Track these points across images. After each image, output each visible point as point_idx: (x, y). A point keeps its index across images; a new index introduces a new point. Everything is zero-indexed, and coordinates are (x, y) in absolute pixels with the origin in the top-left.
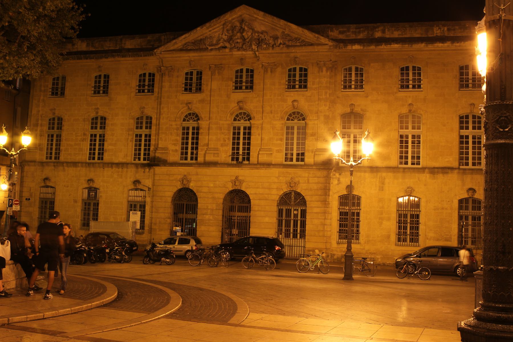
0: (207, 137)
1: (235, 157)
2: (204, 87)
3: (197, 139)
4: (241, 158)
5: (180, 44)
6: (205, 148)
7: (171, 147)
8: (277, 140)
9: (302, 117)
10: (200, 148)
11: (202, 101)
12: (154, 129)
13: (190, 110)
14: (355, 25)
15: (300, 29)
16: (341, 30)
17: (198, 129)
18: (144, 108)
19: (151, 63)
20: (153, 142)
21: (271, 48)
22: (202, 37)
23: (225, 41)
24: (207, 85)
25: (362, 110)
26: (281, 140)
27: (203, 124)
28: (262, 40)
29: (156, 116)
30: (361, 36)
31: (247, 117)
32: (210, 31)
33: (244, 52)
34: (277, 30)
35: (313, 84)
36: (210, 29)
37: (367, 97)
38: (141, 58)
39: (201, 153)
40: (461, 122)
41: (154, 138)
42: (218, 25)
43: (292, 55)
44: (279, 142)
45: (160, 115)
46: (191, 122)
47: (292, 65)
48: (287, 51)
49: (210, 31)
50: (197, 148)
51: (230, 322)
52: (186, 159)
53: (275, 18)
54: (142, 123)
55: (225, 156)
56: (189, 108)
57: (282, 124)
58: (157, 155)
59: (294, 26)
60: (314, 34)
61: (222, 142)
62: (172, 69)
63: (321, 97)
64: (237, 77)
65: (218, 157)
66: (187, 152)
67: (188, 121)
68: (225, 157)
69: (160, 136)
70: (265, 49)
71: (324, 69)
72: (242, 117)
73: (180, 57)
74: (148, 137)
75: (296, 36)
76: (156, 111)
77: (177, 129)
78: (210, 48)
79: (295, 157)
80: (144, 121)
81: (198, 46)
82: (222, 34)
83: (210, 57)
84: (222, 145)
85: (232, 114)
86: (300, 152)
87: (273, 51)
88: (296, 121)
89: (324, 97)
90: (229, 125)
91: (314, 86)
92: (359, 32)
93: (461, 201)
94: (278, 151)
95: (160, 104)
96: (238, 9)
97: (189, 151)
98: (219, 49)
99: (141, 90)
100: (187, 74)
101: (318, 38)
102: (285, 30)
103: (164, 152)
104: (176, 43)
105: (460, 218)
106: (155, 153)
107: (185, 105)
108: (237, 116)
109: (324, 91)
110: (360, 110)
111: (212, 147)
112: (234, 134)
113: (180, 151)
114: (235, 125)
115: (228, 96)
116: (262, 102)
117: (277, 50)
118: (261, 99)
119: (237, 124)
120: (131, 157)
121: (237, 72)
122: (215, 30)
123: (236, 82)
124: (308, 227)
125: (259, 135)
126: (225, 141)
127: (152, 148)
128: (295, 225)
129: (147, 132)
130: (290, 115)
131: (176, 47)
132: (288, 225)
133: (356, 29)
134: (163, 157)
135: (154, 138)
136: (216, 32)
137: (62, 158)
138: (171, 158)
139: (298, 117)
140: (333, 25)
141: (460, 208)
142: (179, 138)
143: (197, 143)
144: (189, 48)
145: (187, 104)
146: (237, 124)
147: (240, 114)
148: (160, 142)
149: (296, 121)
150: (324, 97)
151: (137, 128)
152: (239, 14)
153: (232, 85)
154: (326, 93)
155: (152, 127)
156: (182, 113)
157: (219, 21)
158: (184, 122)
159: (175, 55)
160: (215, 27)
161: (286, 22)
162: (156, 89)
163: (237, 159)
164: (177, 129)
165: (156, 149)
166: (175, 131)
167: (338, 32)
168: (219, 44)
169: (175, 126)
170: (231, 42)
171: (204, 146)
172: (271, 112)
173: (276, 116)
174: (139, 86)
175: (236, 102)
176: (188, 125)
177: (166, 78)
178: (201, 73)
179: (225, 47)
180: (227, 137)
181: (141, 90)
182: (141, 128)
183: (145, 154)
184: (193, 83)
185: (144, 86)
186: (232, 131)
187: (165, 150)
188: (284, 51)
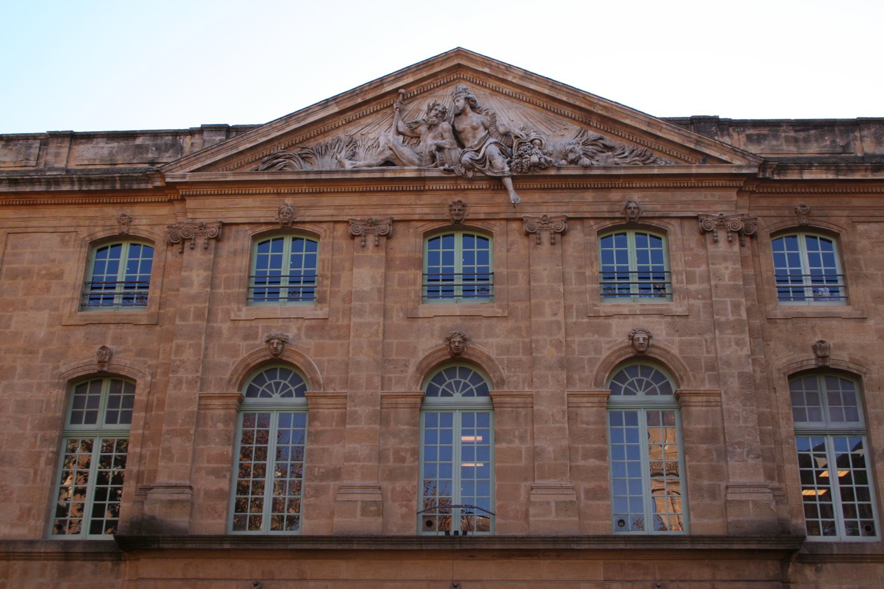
8: (585, 457)
24: (335, 280)
35: (690, 279)
44: (593, 462)
63: (723, 319)
66: (797, 256)
68: (403, 517)
71: (722, 235)
89: (731, 317)
91: (693, 287)
120: (47, 521)
125: (522, 438)
126: (403, 460)
139: (648, 384)
165: (144, 491)
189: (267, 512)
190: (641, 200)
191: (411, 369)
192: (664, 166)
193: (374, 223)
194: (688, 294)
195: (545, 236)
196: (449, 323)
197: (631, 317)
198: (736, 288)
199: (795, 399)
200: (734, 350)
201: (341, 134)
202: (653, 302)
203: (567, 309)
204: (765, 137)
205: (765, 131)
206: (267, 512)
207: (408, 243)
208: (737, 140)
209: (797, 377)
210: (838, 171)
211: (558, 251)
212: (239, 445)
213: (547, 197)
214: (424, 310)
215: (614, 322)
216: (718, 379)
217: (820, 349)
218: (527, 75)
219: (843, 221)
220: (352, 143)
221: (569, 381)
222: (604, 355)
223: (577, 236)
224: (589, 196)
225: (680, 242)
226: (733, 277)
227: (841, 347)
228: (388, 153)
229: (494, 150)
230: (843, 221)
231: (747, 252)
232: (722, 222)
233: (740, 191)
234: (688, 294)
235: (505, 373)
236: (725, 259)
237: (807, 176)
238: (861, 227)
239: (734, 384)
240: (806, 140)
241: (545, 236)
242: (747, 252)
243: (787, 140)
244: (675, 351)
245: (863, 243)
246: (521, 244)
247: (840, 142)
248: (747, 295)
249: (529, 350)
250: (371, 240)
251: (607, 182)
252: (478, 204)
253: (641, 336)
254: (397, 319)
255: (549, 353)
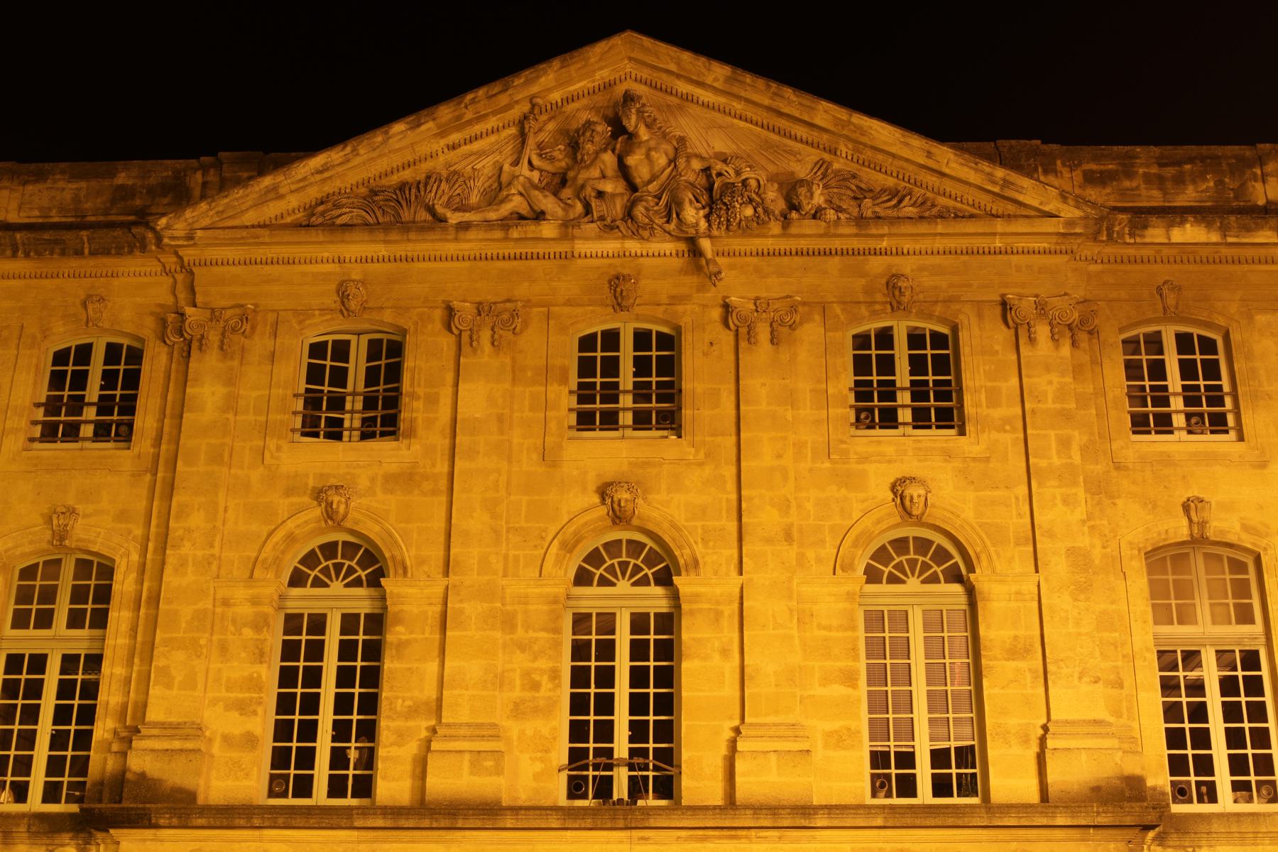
0: (433, 667)
1: (587, 777)
2: (412, 410)
3: (372, 677)
4: (621, 777)
5: (293, 201)
6: (422, 725)
7: (221, 722)
8: (826, 681)
9: (952, 563)
10: (387, 725)
11: (406, 479)
12: (124, 627)
13: (339, 526)
14: (1155, 150)
15: (917, 142)
16: (1093, 166)
17: (376, 622)
18: (72, 511)
19: (127, 294)
20: (109, 697)
21: (775, 228)
22: (407, 175)
23: (536, 187)
24: (432, 400)
25: (1245, 528)
26: (849, 679)
27: (411, 597)
28: (728, 187)
29: (135, 557)
30: (1189, 196)
31: (649, 562)
32: (454, 147)
33: (633, 246)
34: (791, 152)
36: (455, 137)
37: (1263, 465)
38: (74, 264)
39: (394, 751)
41: (120, 671)
42: (492, 122)
43: (877, 265)
44: (838, 690)
45: (162, 549)
46: (337, 587)
47: (874, 314)
48: (856, 244)
49: (454, 147)
50: (368, 731)
52: (304, 787)
53: (788, 92)
54: (49, 595)
55: (538, 767)
56: (330, 514)
57: (850, 596)
58: (137, 763)
59: (883, 133)
60: (985, 166)
61: (517, 693)
62: (244, 318)
63: (1043, 463)
64: (586, 367)
65: (498, 771)
67: (318, 583)
68: (536, 776)
69: (158, 662)
70: (745, 229)
72: (624, 565)
73: (290, 262)
74: (82, 676)
75: (890, 182)
76: (138, 531)
77: (259, 624)
78: (454, 218)
79: (924, 772)
80: (66, 582)
81: (397, 208)
82: (516, 163)
83: (445, 266)
84: (518, 711)
85: (568, 547)
86: (953, 744)
87: (783, 244)
88: (913, 584)
90: (555, 601)
91: (997, 413)
92: (1180, 181)
94: (839, 740)
95: (170, 488)
96: (600, 47)
97: (324, 745)
98: (505, 224)
99: (57, 425)
100: (317, 350)
101: (1006, 183)
102: (833, 152)
103: (177, 744)
104: (274, 193)
106: (124, 754)
107: (306, 499)
108: (594, 558)
109: (1052, 433)
110: (1237, 527)
111: (464, 719)
112: (580, 650)
113: (267, 745)
114: (585, 606)
115: (548, 457)
116: (731, 485)
117: (807, 232)
118: (730, 472)
119: (593, 599)
121: (587, 343)
122: (476, 146)
123: (585, 392)
125: (725, 652)
126: (536, 686)
127: (102, 729)
129: (80, 641)
130: (881, 555)
131: (272, 210)
133: (1161, 165)
134: (173, 774)
135: (120, 671)
136: (481, 154)
138: (215, 783)
140: (1055, 147)
142: (269, 674)
143: (370, 704)
144: (344, 219)
145: (319, 494)
146: (593, 599)
147: (613, 547)
148: (154, 691)
149: (913, 584)
150: (1056, 461)
151: (20, 621)
152: (603, 75)
153: (565, 401)
154: (1065, 443)
155: (113, 615)
156: (291, 539)
157: (503, 99)
158: (296, 591)
159: (271, 249)
160: (478, 128)
161: (842, 113)
162: (145, 420)
163: (604, 790)
164: (259, 624)
165: (129, 734)
166: (248, 633)
167: (1078, 175)
168: (506, 199)
169: (246, 610)
170: (567, 193)
171: (413, 712)
172: (788, 537)
173: (811, 554)
174: (52, 406)
175: (592, 487)
176: (317, 607)
177: (207, 364)
178: (396, 349)
179: (539, 216)
180: (543, 664)
181: (57, 425)
182: (45, 620)
183: (55, 766)
184: (357, 391)
185: (77, 404)
186: (567, 638)
187: (187, 738)
188: (837, 244)
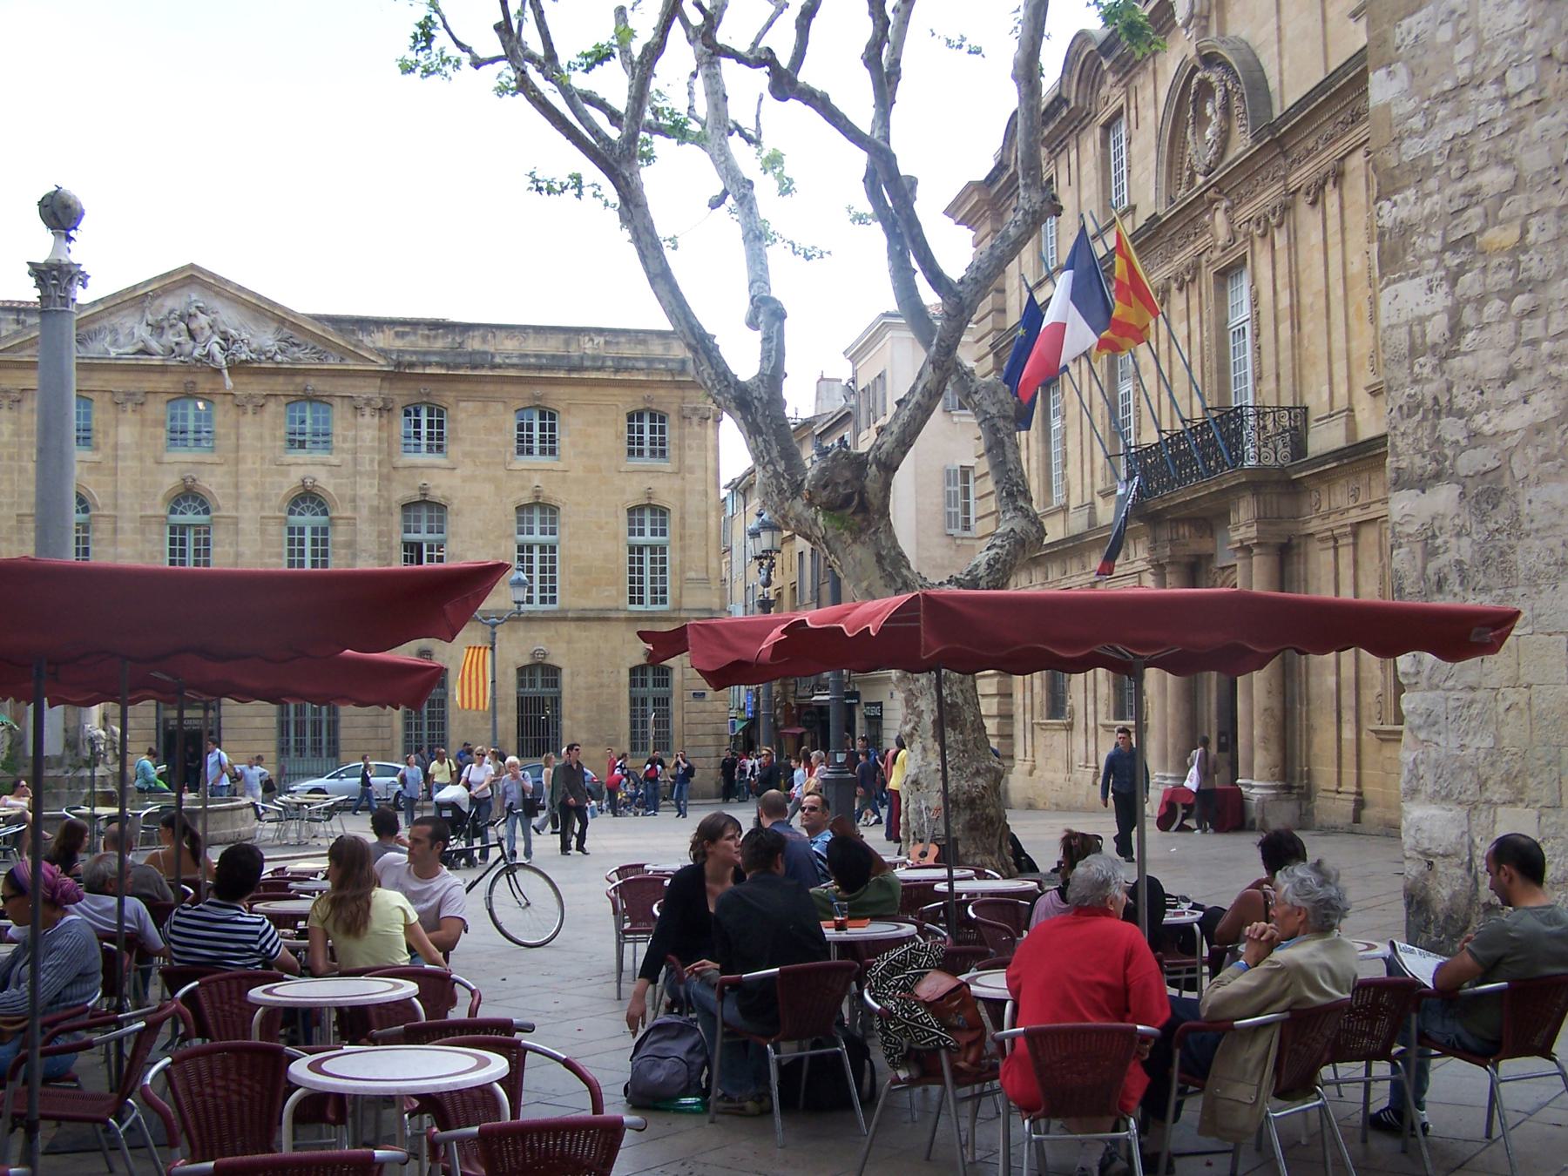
8: (270, 556)
24: (106, 434)
35: (345, 440)
40: (631, 522)
51: (652, 316)
71: (368, 411)
93: (633, 671)
105: (633, 701)
124: (343, 734)
128: (317, 731)
132: (300, 730)
137: (1362, 1085)
141: (633, 683)
189: (308, 558)
190: (314, 384)
191: (159, 499)
192: (333, 363)
193: (134, 394)
194: (343, 450)
195: (250, 408)
196: (184, 467)
197: (307, 467)
198: (373, 448)
199: (406, 518)
200: (368, 489)
201: (105, 323)
202: (320, 456)
203: (263, 458)
204: (407, 334)
205: (407, 329)
206: (308, 558)
207: (157, 408)
208: (382, 340)
209: (406, 507)
210: (448, 368)
211: (258, 418)
212: (286, 558)
213: (252, 379)
214: (168, 457)
215: (292, 468)
216: (355, 508)
217: (424, 490)
218: (240, 288)
219: (451, 400)
220: (114, 331)
221: (262, 508)
222: (285, 491)
223: (272, 406)
224: (281, 379)
225: (340, 411)
226: (372, 440)
227: (437, 487)
228: (140, 345)
229: (216, 349)
230: (451, 400)
231: (384, 421)
232: (368, 402)
233: (383, 379)
234: (343, 450)
235: (221, 502)
236: (368, 427)
237: (428, 371)
238: (462, 404)
239: (365, 512)
240: (435, 337)
241: (250, 408)
242: (384, 421)
243: (423, 336)
244: (330, 490)
245: (462, 416)
246: (233, 413)
247: (458, 339)
248: (380, 452)
249: (236, 486)
250: (129, 406)
251: (292, 373)
252: (204, 385)
253: (308, 482)
254: (149, 463)
255: (249, 490)
